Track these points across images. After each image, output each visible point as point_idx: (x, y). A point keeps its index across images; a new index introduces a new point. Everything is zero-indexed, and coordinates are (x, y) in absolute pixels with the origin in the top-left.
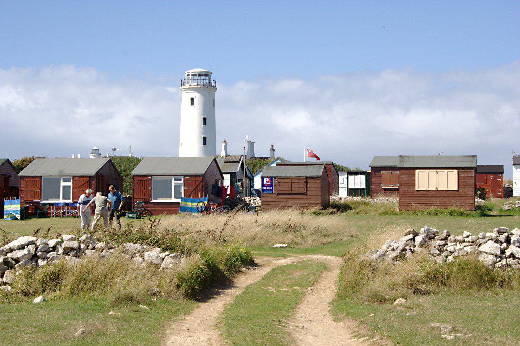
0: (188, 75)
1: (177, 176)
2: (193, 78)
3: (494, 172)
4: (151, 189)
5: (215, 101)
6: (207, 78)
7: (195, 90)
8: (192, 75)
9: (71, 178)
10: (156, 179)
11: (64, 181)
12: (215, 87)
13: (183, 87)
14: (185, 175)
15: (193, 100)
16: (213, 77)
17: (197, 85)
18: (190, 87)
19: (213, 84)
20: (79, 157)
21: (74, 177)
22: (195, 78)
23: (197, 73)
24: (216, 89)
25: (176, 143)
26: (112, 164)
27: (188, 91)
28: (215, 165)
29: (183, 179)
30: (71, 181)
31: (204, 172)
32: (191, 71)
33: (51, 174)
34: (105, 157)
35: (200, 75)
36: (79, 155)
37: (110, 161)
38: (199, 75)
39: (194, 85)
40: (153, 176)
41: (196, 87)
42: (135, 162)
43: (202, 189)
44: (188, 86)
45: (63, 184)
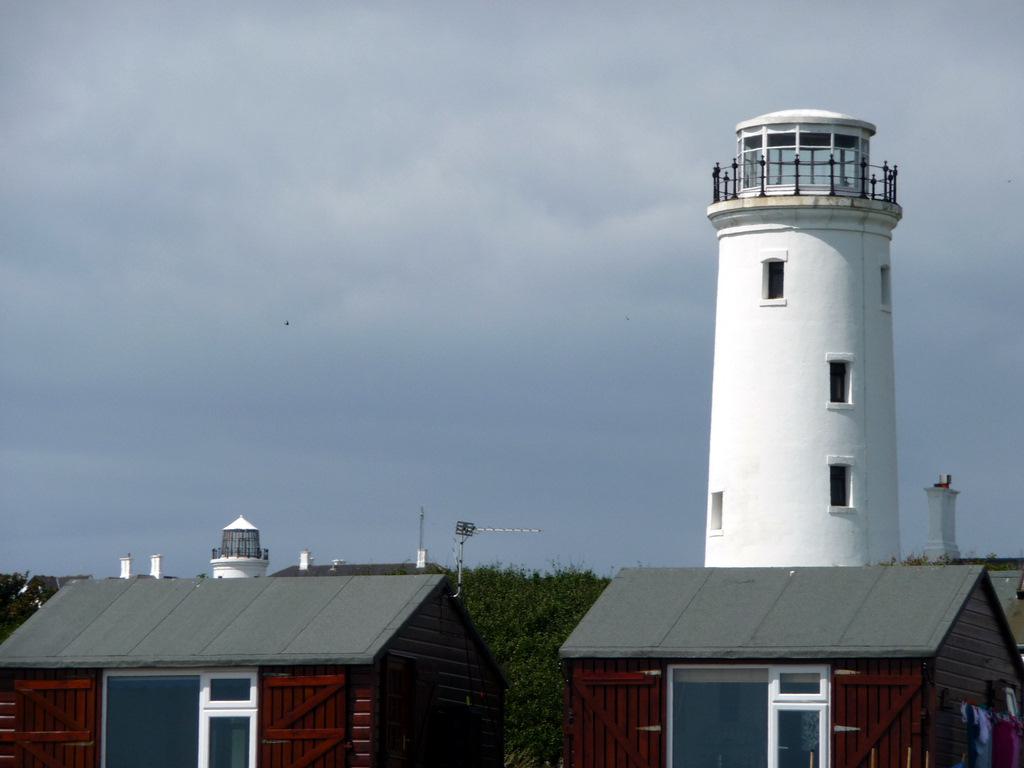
0: (754, 142)
1: (797, 666)
2: (775, 158)
3: (346, 578)
4: (662, 735)
5: (894, 274)
6: (850, 155)
7: (790, 217)
8: (774, 140)
9: (253, 677)
10: (685, 679)
11: (220, 692)
12: (890, 199)
13: (723, 206)
14: (835, 662)
15: (775, 273)
16: (880, 152)
17: (797, 193)
18: (762, 202)
19: (880, 188)
20: (155, 572)
21: (266, 671)
22: (789, 157)
23: (796, 131)
24: (899, 216)
25: (688, 495)
26: (456, 607)
27: (841, 225)
28: (986, 611)
29: (825, 685)
30: (254, 691)
31: (933, 645)
32: (765, 121)
33: (150, 659)
34: (406, 569)
35: (814, 138)
36: (155, 563)
37: (445, 588)
38: (806, 139)
39: (781, 193)
40: (671, 669)
41: (794, 201)
42: (577, 592)
43: (923, 734)
44: (749, 196)
45: (209, 708)
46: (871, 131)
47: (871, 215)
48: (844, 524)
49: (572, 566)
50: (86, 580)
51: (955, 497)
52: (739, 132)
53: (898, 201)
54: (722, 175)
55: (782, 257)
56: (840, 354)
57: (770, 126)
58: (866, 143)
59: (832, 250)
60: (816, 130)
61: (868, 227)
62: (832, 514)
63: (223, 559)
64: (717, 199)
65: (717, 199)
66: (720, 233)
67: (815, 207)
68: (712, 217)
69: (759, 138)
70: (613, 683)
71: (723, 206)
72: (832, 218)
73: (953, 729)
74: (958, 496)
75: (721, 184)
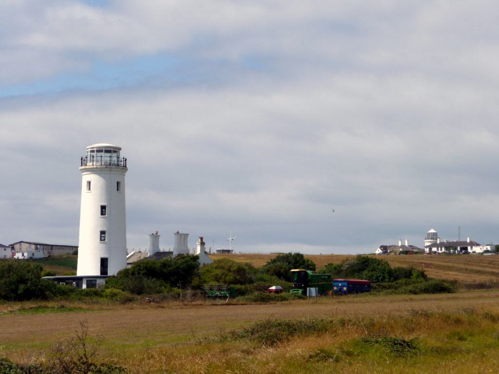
0: (93, 151)
12: (125, 166)
13: (83, 167)
16: (122, 154)
19: (122, 163)
23: (95, 149)
24: (127, 170)
36: (406, 242)
46: (120, 149)
47: (112, 169)
48: (103, 245)
49: (240, 252)
50: (487, 244)
51: (187, 237)
52: (88, 149)
53: (127, 166)
54: (83, 159)
55: (90, 181)
56: (104, 204)
57: (90, 148)
58: (119, 152)
59: (102, 178)
60: (100, 149)
61: (112, 172)
62: (100, 243)
63: (427, 240)
64: (82, 165)
65: (82, 165)
66: (83, 174)
67: (97, 168)
68: (81, 170)
69: (94, 151)
70: (491, 266)
71: (83, 167)
72: (102, 171)
73: (332, 283)
74: (189, 236)
75: (83, 161)
